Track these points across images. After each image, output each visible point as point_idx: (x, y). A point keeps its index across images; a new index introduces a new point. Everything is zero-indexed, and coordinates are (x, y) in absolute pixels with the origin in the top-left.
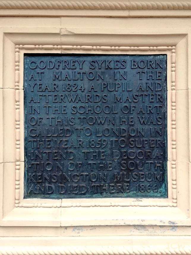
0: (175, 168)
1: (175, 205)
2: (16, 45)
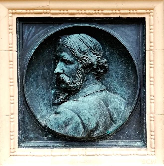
0: (154, 102)
1: (153, 153)
2: (9, 10)
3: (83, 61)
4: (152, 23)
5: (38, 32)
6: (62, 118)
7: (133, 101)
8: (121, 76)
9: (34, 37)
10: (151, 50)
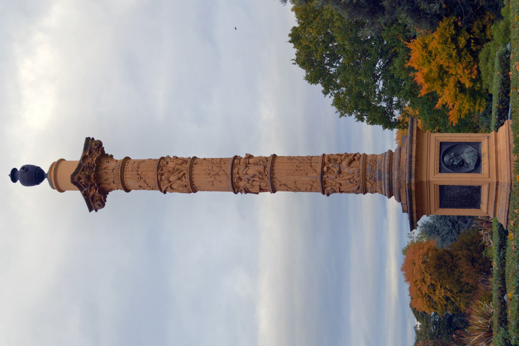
6: (471, 161)
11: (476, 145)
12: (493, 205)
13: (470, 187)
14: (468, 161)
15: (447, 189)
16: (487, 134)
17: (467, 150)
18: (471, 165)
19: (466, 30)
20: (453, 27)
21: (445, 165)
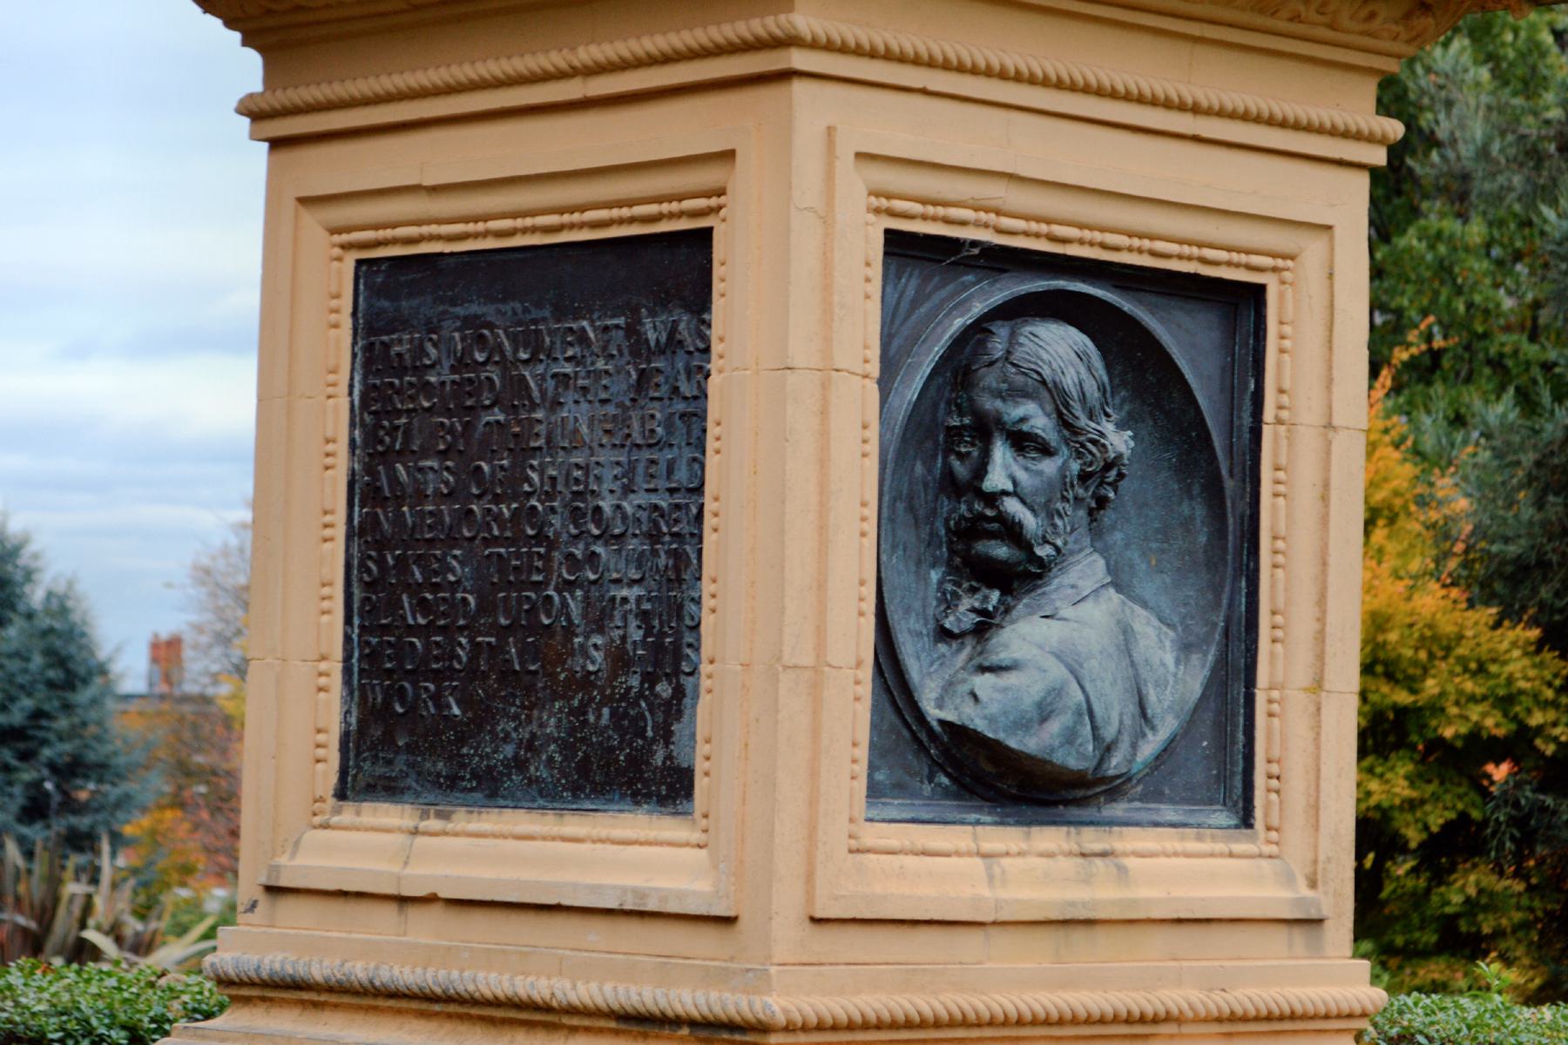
1: (1273, 849)
3: (1089, 445)
4: (1289, 314)
5: (929, 296)
6: (1026, 687)
7: (1210, 633)
8: (1157, 525)
9: (914, 318)
10: (1279, 421)
11: (1219, 765)
12: (406, 975)
13: (669, 649)
14: (1026, 636)
15: (639, 347)
16: (1338, 900)
17: (1157, 645)
18: (984, 684)
19: (1464, 816)
20: (1494, 724)
21: (979, 329)
